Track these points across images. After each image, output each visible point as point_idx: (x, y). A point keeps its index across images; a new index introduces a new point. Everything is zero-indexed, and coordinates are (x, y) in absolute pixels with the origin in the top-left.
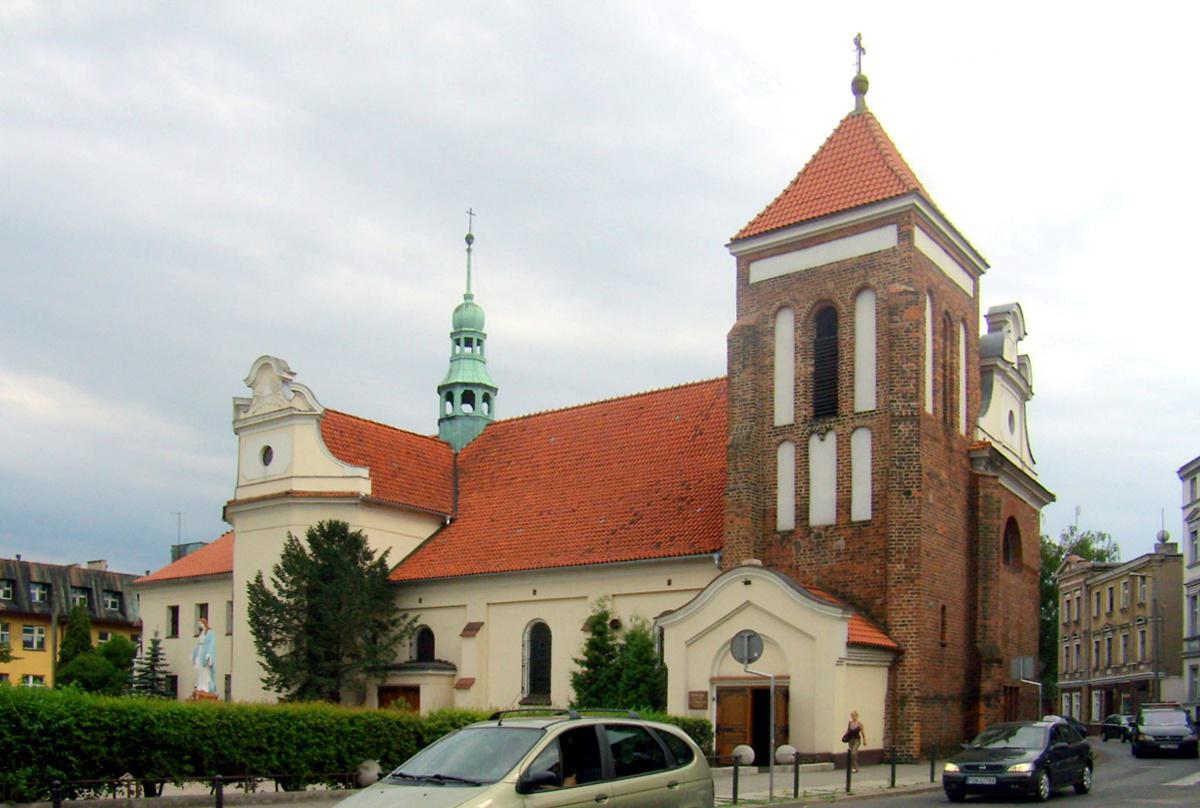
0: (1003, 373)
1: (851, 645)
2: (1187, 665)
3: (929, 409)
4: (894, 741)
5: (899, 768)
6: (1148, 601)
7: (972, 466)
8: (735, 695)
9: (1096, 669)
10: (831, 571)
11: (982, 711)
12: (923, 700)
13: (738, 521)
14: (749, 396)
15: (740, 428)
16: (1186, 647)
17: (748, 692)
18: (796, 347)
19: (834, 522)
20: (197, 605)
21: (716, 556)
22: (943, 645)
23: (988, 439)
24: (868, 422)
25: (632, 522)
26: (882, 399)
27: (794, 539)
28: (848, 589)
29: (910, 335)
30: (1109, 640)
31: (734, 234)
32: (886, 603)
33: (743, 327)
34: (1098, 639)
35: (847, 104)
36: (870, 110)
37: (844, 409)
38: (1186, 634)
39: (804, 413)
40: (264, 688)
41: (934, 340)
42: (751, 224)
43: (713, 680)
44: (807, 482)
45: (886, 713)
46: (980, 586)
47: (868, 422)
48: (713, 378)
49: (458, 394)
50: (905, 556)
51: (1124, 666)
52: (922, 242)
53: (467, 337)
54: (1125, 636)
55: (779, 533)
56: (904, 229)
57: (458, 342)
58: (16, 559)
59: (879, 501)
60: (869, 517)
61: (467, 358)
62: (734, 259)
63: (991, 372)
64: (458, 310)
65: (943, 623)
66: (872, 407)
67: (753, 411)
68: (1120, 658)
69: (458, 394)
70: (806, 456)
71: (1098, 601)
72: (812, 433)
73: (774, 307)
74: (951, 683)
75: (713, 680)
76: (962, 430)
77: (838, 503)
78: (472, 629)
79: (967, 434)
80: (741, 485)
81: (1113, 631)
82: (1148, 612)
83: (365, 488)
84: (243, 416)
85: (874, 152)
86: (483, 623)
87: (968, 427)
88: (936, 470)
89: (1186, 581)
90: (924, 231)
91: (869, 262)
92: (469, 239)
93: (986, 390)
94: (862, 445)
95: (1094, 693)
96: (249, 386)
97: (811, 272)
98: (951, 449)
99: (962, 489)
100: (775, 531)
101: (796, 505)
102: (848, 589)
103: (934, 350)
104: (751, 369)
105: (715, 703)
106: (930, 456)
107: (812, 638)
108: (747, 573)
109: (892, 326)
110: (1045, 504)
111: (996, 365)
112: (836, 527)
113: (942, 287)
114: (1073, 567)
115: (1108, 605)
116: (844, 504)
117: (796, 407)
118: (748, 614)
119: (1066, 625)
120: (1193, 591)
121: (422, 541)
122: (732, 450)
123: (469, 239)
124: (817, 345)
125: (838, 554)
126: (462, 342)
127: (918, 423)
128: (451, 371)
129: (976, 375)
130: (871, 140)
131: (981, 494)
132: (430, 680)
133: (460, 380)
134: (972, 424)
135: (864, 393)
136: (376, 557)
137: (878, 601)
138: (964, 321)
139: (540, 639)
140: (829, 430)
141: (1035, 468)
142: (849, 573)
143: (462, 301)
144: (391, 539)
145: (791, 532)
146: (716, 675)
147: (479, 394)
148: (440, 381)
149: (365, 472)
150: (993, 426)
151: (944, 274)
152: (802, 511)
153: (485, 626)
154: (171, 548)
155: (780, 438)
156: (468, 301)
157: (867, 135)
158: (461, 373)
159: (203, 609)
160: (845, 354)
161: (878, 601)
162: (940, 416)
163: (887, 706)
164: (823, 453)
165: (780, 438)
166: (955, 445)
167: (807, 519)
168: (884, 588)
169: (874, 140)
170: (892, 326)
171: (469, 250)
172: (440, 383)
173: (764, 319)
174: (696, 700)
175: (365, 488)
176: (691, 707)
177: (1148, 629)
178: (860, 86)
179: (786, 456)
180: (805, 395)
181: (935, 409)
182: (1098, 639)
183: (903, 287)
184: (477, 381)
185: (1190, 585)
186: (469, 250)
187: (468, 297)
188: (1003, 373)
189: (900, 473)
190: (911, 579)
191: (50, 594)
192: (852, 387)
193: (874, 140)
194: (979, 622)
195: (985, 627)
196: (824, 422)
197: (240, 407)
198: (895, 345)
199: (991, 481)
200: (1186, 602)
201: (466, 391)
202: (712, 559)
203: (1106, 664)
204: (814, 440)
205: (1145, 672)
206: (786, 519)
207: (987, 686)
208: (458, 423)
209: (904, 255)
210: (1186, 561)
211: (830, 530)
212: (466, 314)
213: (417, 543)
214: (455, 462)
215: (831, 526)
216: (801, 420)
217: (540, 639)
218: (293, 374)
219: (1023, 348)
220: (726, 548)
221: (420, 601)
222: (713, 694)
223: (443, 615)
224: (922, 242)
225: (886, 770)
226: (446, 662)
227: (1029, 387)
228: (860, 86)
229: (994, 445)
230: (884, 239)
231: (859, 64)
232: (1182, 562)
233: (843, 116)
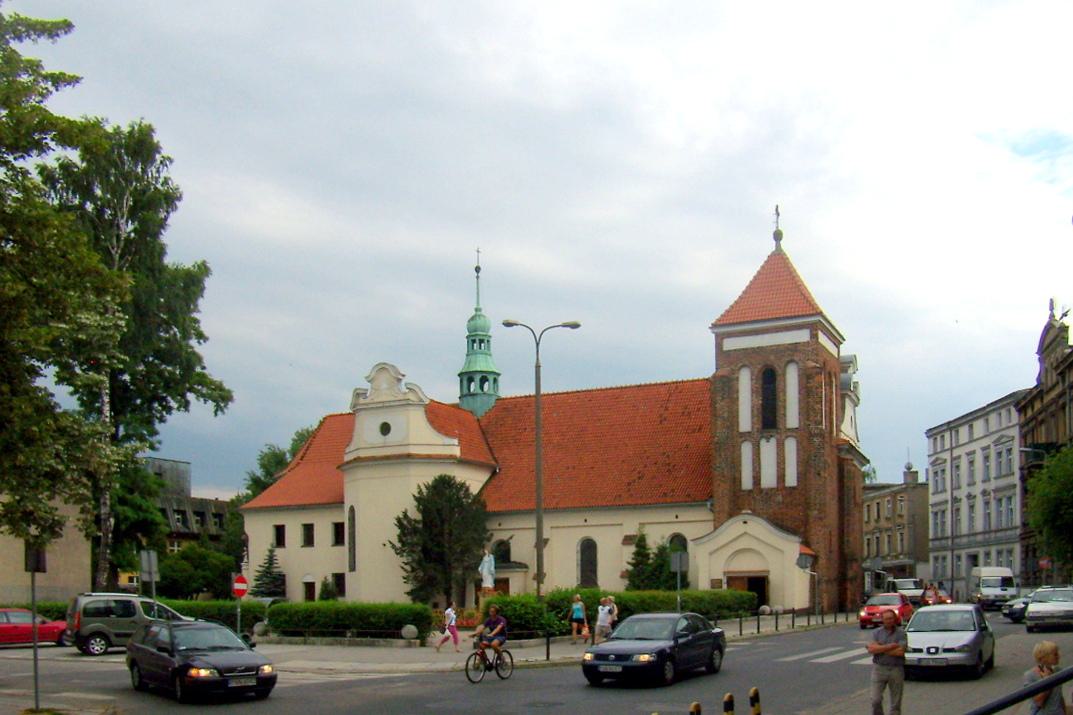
0: (850, 396)
2: (931, 556)
6: (904, 512)
9: (868, 557)
13: (722, 484)
14: (726, 415)
16: (931, 544)
17: (746, 580)
18: (752, 390)
21: (709, 504)
25: (639, 478)
30: (877, 538)
31: (713, 321)
34: (869, 537)
38: (931, 536)
43: (725, 573)
44: (759, 464)
47: (794, 434)
51: (888, 555)
52: (823, 339)
53: (477, 339)
54: (889, 536)
59: (801, 476)
62: (713, 335)
64: (473, 318)
66: (797, 426)
68: (885, 549)
71: (869, 511)
72: (762, 437)
75: (725, 573)
81: (881, 532)
82: (905, 520)
83: (457, 452)
84: (361, 401)
89: (931, 502)
92: (478, 269)
93: (843, 408)
94: (791, 446)
95: (866, 573)
97: (760, 349)
100: (740, 490)
107: (782, 551)
108: (746, 518)
112: (777, 489)
115: (876, 514)
116: (781, 477)
117: (753, 423)
120: (936, 509)
123: (478, 269)
133: (479, 369)
134: (839, 430)
135: (792, 417)
139: (588, 550)
141: (858, 444)
142: (787, 512)
143: (474, 313)
145: (750, 491)
149: (456, 442)
152: (757, 480)
153: (549, 542)
159: (309, 530)
164: (768, 449)
171: (478, 277)
172: (459, 372)
173: (733, 372)
174: (716, 583)
175: (457, 452)
177: (906, 531)
178: (778, 236)
179: (746, 449)
182: (869, 537)
183: (814, 364)
185: (932, 506)
186: (478, 277)
190: (821, 519)
191: (221, 520)
192: (785, 415)
194: (846, 539)
195: (848, 541)
198: (807, 392)
200: (931, 516)
202: (706, 505)
203: (875, 554)
204: (763, 442)
205: (904, 560)
206: (747, 483)
210: (931, 489)
214: (480, 427)
217: (588, 550)
218: (403, 376)
220: (715, 499)
221: (500, 525)
222: (725, 580)
224: (823, 339)
227: (859, 400)
228: (778, 236)
230: (803, 336)
231: (777, 222)
232: (928, 489)
233: (769, 254)
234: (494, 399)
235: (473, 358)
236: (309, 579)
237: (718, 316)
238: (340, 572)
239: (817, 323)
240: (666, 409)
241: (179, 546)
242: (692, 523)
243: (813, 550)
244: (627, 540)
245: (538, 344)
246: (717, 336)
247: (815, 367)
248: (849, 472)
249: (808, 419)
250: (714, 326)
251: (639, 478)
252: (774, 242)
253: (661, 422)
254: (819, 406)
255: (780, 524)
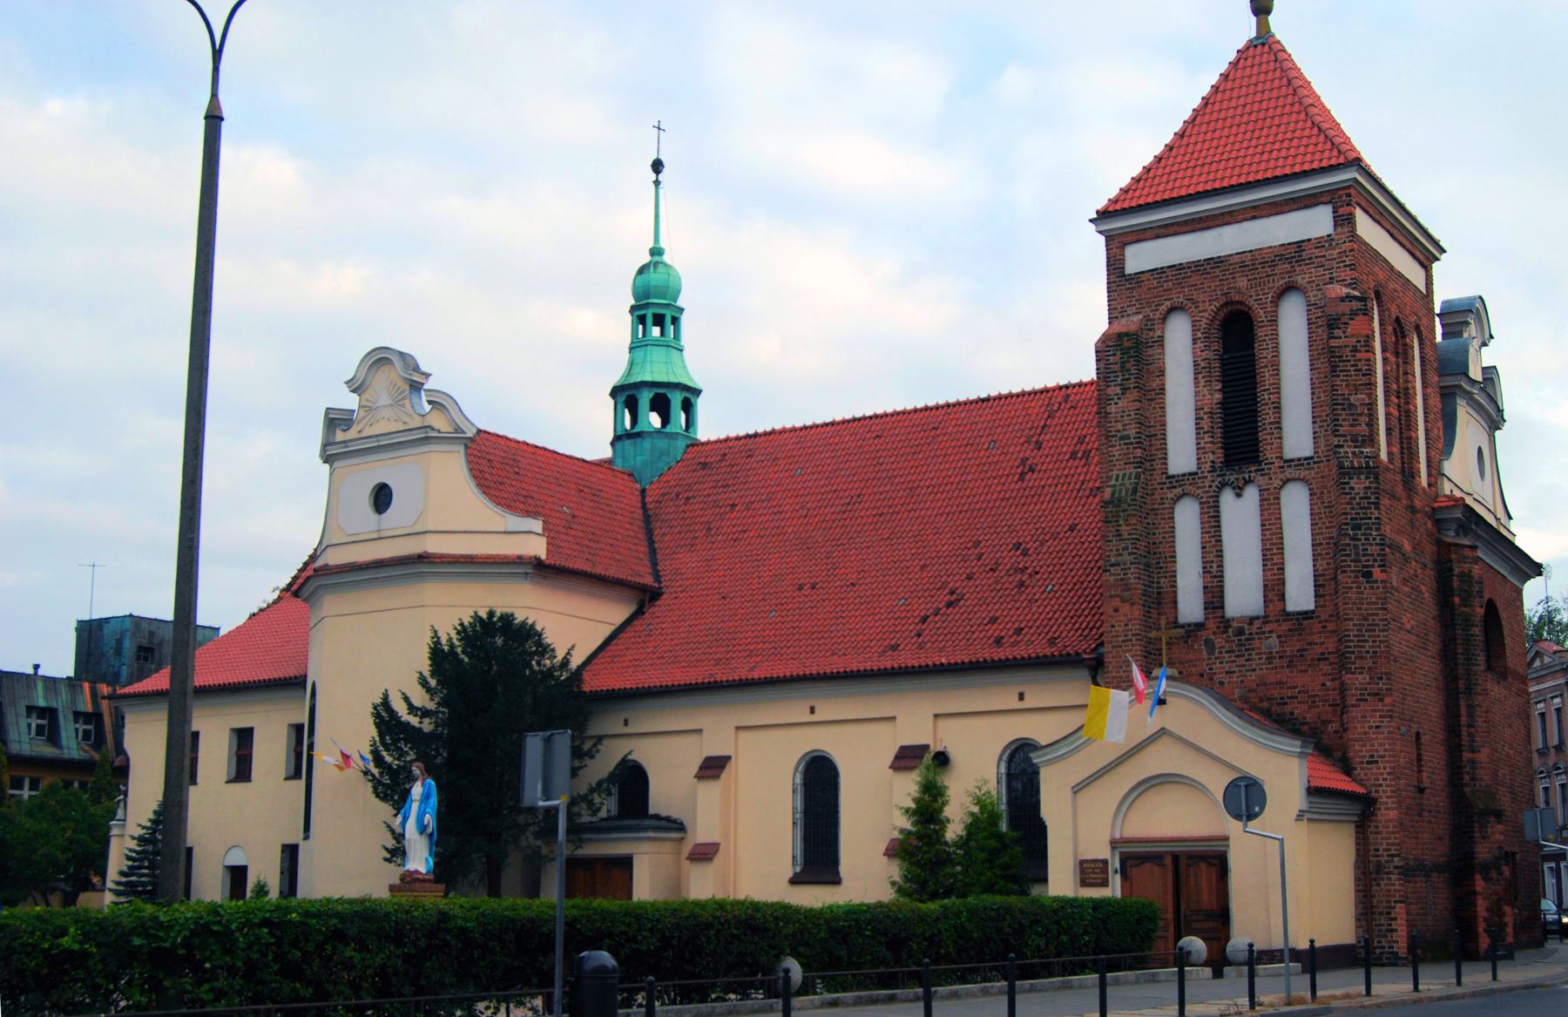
0: (1469, 397)
1: (1313, 792)
3: (1384, 456)
4: (1369, 930)
5: (1375, 972)
7: (1439, 531)
8: (1148, 865)
10: (1262, 683)
11: (1478, 889)
12: (1406, 872)
13: (1125, 608)
14: (1132, 432)
15: (1122, 477)
18: (1196, 364)
19: (1262, 613)
20: (233, 730)
22: (1421, 791)
23: (1458, 494)
24: (1304, 473)
25: (950, 604)
26: (1322, 442)
27: (1203, 634)
28: (1287, 709)
29: (1359, 355)
31: (1101, 204)
32: (1345, 730)
33: (1120, 336)
35: (1247, 28)
36: (1278, 37)
37: (1268, 454)
39: (1212, 457)
40: (386, 859)
41: (1385, 360)
42: (1124, 191)
44: (1220, 554)
45: (1357, 891)
46: (1463, 703)
47: (1304, 473)
48: (1039, 386)
49: (645, 398)
50: (1368, 663)
52: (1367, 228)
53: (655, 311)
55: (1182, 626)
56: (1341, 211)
57: (642, 320)
58: (31, 671)
59: (1321, 584)
60: (1312, 607)
61: (656, 344)
62: (1102, 239)
63: (1453, 395)
64: (642, 271)
65: (1419, 759)
67: (1139, 452)
69: (645, 398)
70: (1217, 517)
72: (1223, 485)
73: (1163, 308)
74: (1432, 844)
75: (1114, 844)
76: (1424, 481)
77: (1265, 586)
78: (713, 767)
79: (1430, 485)
80: (1127, 558)
84: (340, 436)
85: (1290, 100)
86: (729, 758)
87: (1429, 475)
88: (1398, 539)
90: (1367, 212)
91: (1297, 252)
92: (657, 166)
94: (1296, 504)
96: (353, 391)
98: (1412, 509)
99: (1430, 565)
101: (1205, 588)
102: (1287, 709)
103: (1385, 373)
104: (1135, 394)
105: (1118, 877)
106: (1392, 523)
109: (1333, 343)
110: (1530, 577)
111: (1460, 387)
112: (1265, 619)
113: (1391, 286)
114: (1547, 660)
116: (1274, 587)
118: (1162, 747)
119: (1543, 753)
121: (613, 628)
122: (1110, 508)
123: (657, 166)
124: (1224, 364)
125: (1270, 658)
126: (649, 320)
127: (1377, 478)
128: (631, 364)
129: (1435, 401)
130: (1285, 81)
131: (1456, 571)
132: (646, 847)
133: (648, 378)
134: (1436, 472)
135: (1297, 431)
136: (560, 655)
137: (1331, 728)
138: (1417, 328)
139: (820, 782)
140: (1248, 482)
142: (1279, 676)
144: (572, 627)
145: (1199, 626)
146: (1118, 836)
147: (676, 399)
148: (615, 378)
149: (537, 525)
150: (1459, 473)
151: (1392, 268)
152: (1214, 595)
154: (75, 625)
155: (1179, 490)
156: (657, 258)
157: (1278, 74)
158: (648, 368)
160: (1266, 376)
161: (1331, 728)
162: (1398, 463)
163: (1357, 879)
164: (1240, 514)
165: (1179, 490)
166: (1418, 504)
167: (1222, 607)
168: (1342, 708)
169: (1289, 82)
170: (1333, 343)
171: (657, 183)
174: (1090, 872)
175: (537, 547)
176: (1084, 883)
179: (1187, 517)
180: (1211, 432)
181: (1390, 454)
183: (1346, 290)
184: (673, 379)
186: (657, 183)
187: (656, 252)
188: (1469, 397)
189: (1356, 547)
192: (1278, 424)
193: (1289, 82)
194: (1466, 755)
196: (1240, 471)
197: (335, 421)
198: (1335, 363)
199: (1468, 552)
201: (656, 395)
204: (1227, 497)
206: (1190, 606)
207: (1483, 852)
208: (647, 444)
209: (1344, 247)
211: (1257, 623)
212: (654, 278)
213: (607, 631)
214: (644, 505)
215: (1258, 618)
216: (1207, 467)
217: (820, 782)
218: (427, 375)
219: (1488, 357)
221: (626, 723)
223: (667, 755)
224: (1367, 228)
225: (1359, 974)
226: (668, 819)
227: (1500, 411)
229: (1469, 501)
230: (1317, 223)
234: (681, 444)
235: (639, 354)
236: (236, 859)
237: (1113, 192)
238: (292, 841)
239: (1352, 188)
240: (1039, 446)
241: (31, 789)
242: (1039, 711)
243: (1360, 782)
244: (907, 758)
245: (217, 54)
246: (1111, 239)
247: (1349, 297)
248: (1466, 577)
249: (1335, 433)
250: (1103, 215)
251: (950, 604)
252: (1254, 19)
253: (1022, 474)
254: (1359, 398)
255: (1269, 712)
